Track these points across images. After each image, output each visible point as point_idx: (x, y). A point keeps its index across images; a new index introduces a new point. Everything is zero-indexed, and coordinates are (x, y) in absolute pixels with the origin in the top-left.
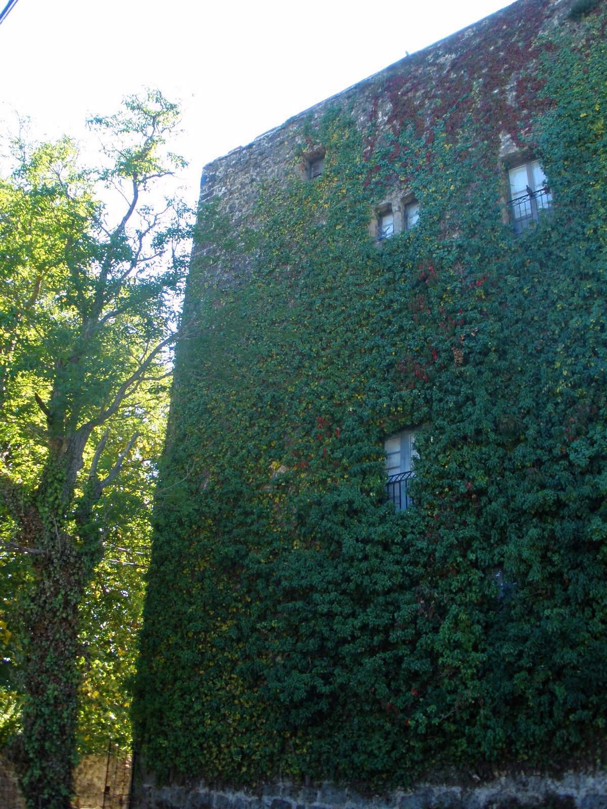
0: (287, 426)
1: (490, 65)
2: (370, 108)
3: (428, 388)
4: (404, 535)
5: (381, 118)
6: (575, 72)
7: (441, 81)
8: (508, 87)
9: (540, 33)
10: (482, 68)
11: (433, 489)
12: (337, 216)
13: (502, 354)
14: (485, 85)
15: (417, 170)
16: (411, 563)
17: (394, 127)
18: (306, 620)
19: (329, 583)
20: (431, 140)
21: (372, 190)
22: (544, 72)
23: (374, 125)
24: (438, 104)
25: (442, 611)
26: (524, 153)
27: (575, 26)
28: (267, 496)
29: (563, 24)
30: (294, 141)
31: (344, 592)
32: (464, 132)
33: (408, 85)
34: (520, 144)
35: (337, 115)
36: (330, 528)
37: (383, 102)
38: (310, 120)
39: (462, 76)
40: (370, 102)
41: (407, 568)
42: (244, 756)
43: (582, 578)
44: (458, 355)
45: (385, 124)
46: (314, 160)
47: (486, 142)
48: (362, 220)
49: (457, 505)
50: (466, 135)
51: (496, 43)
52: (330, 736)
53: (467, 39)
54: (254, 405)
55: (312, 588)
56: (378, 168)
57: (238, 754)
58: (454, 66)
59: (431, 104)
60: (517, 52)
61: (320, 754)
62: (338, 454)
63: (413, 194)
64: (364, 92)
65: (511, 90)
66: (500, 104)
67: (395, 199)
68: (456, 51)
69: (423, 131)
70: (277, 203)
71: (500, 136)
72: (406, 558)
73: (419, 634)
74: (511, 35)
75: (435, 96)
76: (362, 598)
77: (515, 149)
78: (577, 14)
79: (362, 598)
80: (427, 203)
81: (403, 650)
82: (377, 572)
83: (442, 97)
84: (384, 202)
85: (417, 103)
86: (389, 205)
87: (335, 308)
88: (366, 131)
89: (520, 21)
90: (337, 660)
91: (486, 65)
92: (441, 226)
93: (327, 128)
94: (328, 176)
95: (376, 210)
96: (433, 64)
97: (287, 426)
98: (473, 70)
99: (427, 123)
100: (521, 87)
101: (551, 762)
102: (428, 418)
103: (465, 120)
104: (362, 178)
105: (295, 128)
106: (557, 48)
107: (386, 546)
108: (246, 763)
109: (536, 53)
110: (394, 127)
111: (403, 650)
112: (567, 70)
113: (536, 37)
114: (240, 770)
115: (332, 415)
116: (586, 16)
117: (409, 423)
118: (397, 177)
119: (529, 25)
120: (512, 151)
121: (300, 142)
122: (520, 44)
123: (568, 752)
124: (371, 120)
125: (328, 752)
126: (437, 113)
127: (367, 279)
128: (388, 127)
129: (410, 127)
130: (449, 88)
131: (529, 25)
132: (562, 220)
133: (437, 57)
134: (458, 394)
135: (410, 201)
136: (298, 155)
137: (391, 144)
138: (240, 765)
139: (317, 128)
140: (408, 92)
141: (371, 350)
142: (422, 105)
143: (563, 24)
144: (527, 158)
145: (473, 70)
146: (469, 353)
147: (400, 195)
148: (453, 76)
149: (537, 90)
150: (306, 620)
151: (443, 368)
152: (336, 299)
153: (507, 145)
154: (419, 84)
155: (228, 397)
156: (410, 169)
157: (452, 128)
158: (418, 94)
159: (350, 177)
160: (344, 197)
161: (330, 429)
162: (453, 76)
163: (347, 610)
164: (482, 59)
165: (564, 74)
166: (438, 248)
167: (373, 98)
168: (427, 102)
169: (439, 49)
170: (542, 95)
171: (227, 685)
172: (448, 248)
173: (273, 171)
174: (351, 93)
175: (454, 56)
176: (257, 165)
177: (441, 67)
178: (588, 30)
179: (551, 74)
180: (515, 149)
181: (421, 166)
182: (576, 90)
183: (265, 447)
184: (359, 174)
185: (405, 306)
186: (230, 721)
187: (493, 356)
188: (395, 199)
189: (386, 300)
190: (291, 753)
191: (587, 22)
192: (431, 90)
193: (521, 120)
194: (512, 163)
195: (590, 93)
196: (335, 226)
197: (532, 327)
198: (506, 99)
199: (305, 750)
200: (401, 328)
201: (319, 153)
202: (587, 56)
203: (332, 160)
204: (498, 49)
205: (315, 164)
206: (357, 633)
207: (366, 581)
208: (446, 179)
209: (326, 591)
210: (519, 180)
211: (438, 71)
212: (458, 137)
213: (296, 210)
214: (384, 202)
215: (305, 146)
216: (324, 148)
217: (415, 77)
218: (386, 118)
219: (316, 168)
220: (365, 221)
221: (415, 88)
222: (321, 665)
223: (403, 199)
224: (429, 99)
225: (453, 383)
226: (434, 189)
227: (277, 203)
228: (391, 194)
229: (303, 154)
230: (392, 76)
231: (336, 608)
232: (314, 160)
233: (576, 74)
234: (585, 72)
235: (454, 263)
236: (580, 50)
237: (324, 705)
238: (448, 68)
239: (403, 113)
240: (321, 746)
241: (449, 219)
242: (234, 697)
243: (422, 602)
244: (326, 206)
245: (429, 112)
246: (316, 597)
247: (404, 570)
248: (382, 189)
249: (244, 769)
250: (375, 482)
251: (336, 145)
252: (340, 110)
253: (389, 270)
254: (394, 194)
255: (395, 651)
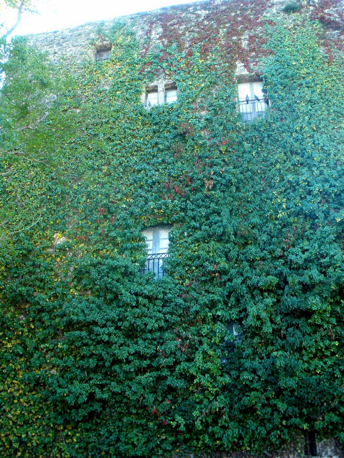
0: (69, 211)
1: (232, 22)
2: (147, 28)
3: (183, 201)
4: (165, 293)
5: (154, 35)
6: (286, 40)
7: (198, 24)
8: (243, 38)
9: (265, 14)
10: (226, 23)
11: (184, 266)
12: (117, 86)
13: (238, 189)
14: (228, 33)
15: (179, 70)
16: (172, 314)
17: (163, 42)
18: (86, 345)
19: (107, 320)
20: (190, 54)
21: (145, 75)
22: (267, 35)
23: (149, 38)
24: (195, 36)
25: (193, 348)
26: (251, 77)
27: (286, 16)
28: (51, 256)
29: (279, 13)
30: (89, 35)
31: (117, 328)
32: (212, 55)
33: (175, 21)
34: (249, 70)
35: (123, 27)
36: (110, 283)
37: (156, 26)
38: (102, 26)
39: (213, 24)
40: (147, 25)
41: (168, 316)
42: (21, 442)
43: (298, 333)
44: (210, 184)
45: (157, 39)
46: (101, 50)
47: (227, 64)
48: (137, 91)
49: (203, 278)
50: (214, 57)
51: (236, 12)
52: (95, 430)
53: (217, 5)
54: (44, 194)
55: (95, 323)
56: (151, 63)
57: (17, 442)
58: (207, 17)
59: (190, 35)
60: (250, 20)
61: (88, 443)
62: (113, 234)
63: (175, 83)
64: (143, 18)
65: (245, 39)
66: (237, 44)
67: (161, 83)
68: (209, 9)
69: (184, 49)
70: (72, 70)
71: (237, 63)
72: (166, 310)
73: (177, 363)
74: (246, 10)
75: (193, 31)
76: (132, 333)
77: (245, 72)
78: (289, 10)
79: (132, 333)
80: (185, 90)
81: (165, 372)
82: (146, 316)
83: (199, 33)
84: (152, 84)
85: (180, 32)
86: (157, 87)
87: (113, 141)
88: (142, 41)
89: (252, 4)
90: (110, 375)
91: (229, 22)
92: (193, 106)
93: (115, 32)
94: (113, 61)
95: (147, 87)
96: (193, 13)
97: (69, 211)
98: (219, 22)
99: (187, 45)
100: (251, 39)
101: (266, 452)
102: (182, 221)
103: (213, 49)
104: (138, 67)
105: (90, 28)
106: (275, 24)
107: (150, 298)
108: (21, 449)
109: (261, 24)
110: (163, 42)
111: (165, 372)
112: (282, 38)
113: (262, 15)
114: (16, 454)
115: (109, 208)
116: (293, 13)
117: (165, 222)
118: (164, 71)
119: (257, 8)
120: (243, 73)
121: (93, 37)
122: (251, 17)
123: (278, 445)
124: (147, 35)
125: (95, 442)
126: (194, 41)
127: (138, 127)
128: (158, 41)
129: (174, 45)
130: (203, 29)
131: (257, 8)
132: (277, 118)
133: (196, 10)
134: (208, 207)
135: (172, 87)
136: (92, 44)
137: (161, 52)
138: (16, 451)
139: (107, 31)
140: (174, 25)
141: (139, 171)
142: (184, 34)
143: (279, 13)
144: (257, 78)
145: (219, 22)
146: (217, 184)
147: (165, 82)
148: (206, 23)
149: (262, 43)
150: (86, 345)
151: (195, 190)
152: (114, 135)
153: (240, 70)
154: (182, 22)
155: (23, 185)
156: (173, 68)
157: (204, 52)
158: (181, 27)
159: (129, 64)
160: (124, 75)
161: (105, 217)
162: (206, 23)
163: (121, 341)
164: (226, 19)
165: (280, 39)
166: (192, 118)
167: (149, 22)
168: (187, 33)
169: (197, 6)
170: (265, 47)
171: (9, 388)
172: (199, 119)
173: (71, 50)
174: (133, 16)
175: (207, 12)
176: (59, 44)
177: (198, 16)
178: (295, 20)
179: (271, 37)
180: (245, 72)
181: (182, 68)
182: (287, 49)
183: (52, 222)
184: (136, 64)
185: (169, 148)
186: (10, 416)
187: (234, 189)
188: (161, 83)
189: (153, 142)
190: (62, 442)
191: (294, 16)
192: (191, 27)
193: (251, 57)
194: (242, 80)
195: (295, 53)
196: (116, 91)
197: (257, 176)
198: (241, 44)
199: (75, 440)
200: (163, 161)
201: (105, 47)
202: (294, 33)
203: (115, 52)
204: (237, 16)
205: (101, 53)
206: (131, 358)
207: (139, 322)
208: (199, 79)
209: (105, 326)
210: (244, 91)
211: (196, 18)
212: (208, 57)
213: (88, 76)
214: (152, 84)
215: (97, 40)
216: (111, 44)
217: (180, 18)
218: (158, 36)
219: (100, 56)
220: (138, 92)
221: (180, 23)
222: (97, 378)
223: (166, 85)
224: (189, 32)
225: (203, 201)
226: (190, 83)
227: (72, 70)
228: (158, 80)
229: (95, 45)
230: (163, 14)
231: (114, 339)
232: (101, 50)
233: (287, 42)
234: (293, 42)
235: (202, 129)
236: (289, 30)
237: (97, 407)
238: (203, 18)
239: (169, 35)
240: (89, 438)
241: (199, 103)
242: (14, 398)
243: (180, 340)
244: (110, 78)
245: (189, 39)
246: (97, 329)
247: (165, 318)
248: (153, 75)
249: (19, 454)
250: (139, 256)
251: (120, 44)
252: (125, 24)
253: (156, 124)
254: (160, 81)
255: (159, 373)
